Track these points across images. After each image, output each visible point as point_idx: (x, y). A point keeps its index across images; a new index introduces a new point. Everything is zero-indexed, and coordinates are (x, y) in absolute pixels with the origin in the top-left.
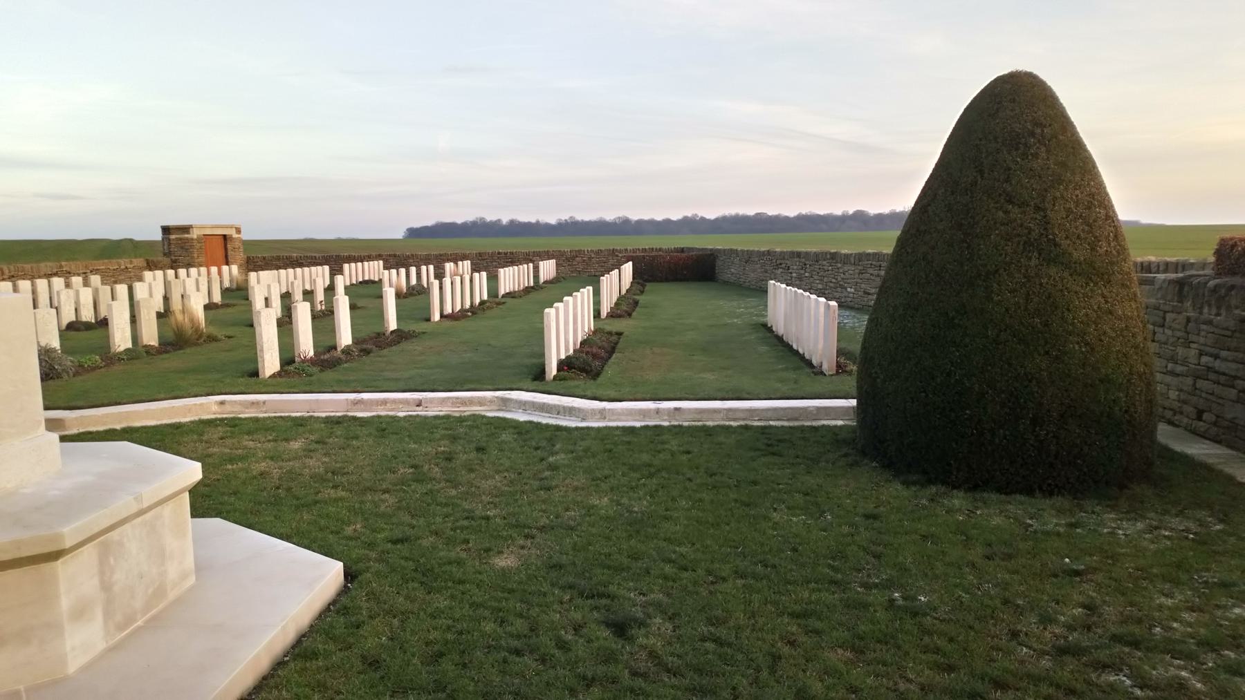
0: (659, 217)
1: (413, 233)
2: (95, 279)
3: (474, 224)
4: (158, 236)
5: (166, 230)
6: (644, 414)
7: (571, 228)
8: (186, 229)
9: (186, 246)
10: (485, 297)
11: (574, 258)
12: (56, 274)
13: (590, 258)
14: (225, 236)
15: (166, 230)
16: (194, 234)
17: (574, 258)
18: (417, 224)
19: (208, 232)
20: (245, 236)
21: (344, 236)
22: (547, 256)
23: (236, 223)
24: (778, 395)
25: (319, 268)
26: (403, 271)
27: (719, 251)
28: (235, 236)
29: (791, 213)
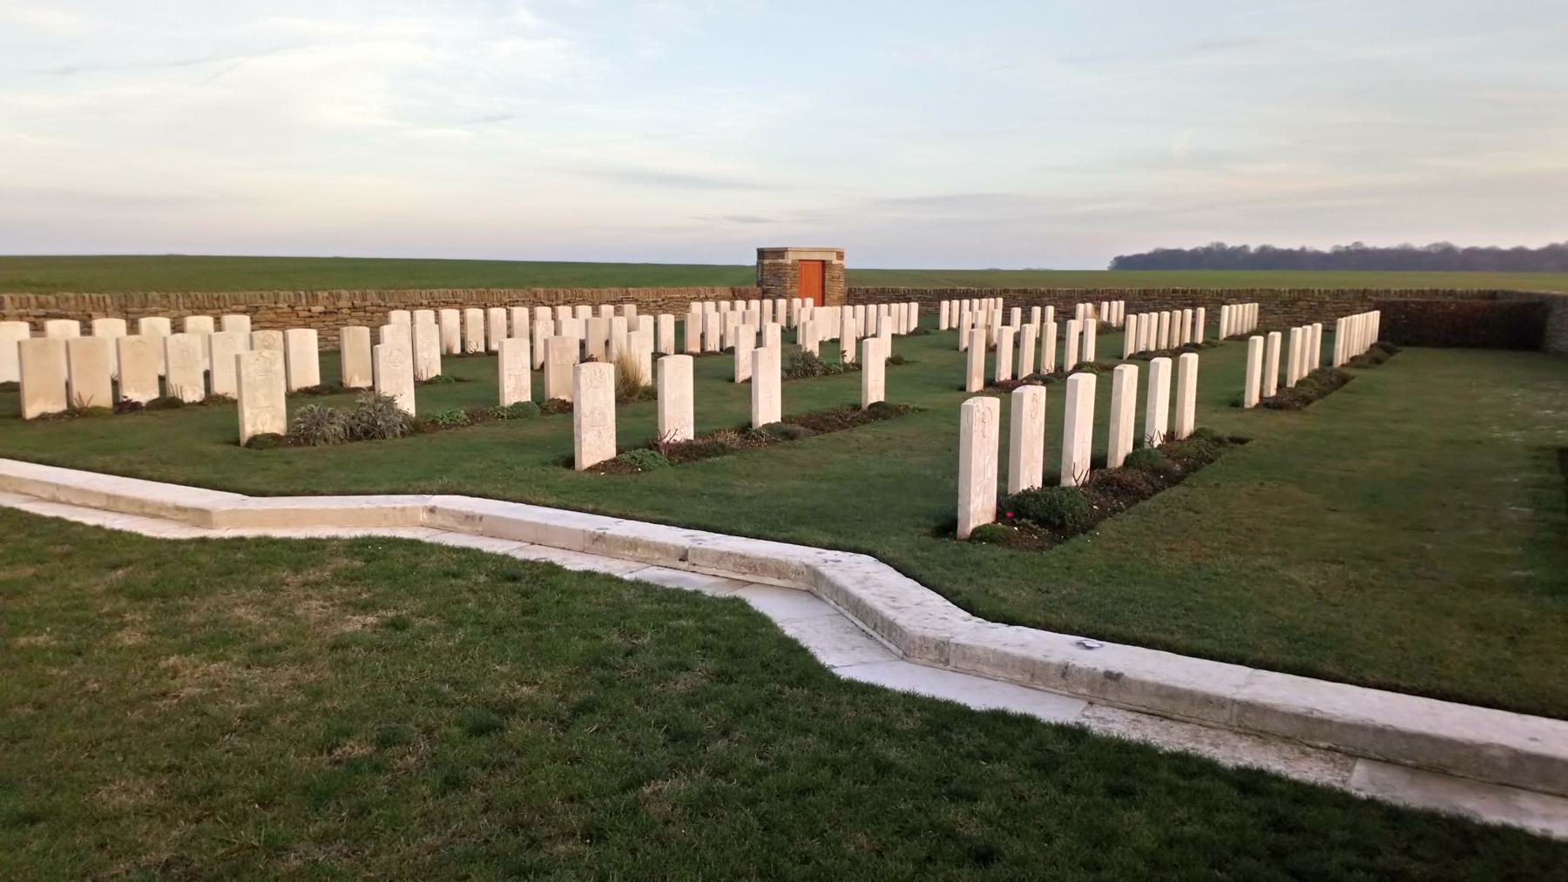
0: (1506, 244)
1: (1123, 263)
2: (630, 309)
3: (1208, 252)
4: (751, 260)
5: (762, 253)
6: (1252, 720)
7: (1269, 259)
8: (780, 253)
9: (778, 273)
10: (1316, 366)
11: (1294, 302)
12: (448, 304)
13: (1322, 304)
15: (762, 253)
16: (790, 259)
17: (1294, 302)
18: (1129, 251)
19: (805, 256)
20: (849, 263)
21: (1034, 267)
22: (1239, 297)
23: (838, 246)
24: (1421, 684)
25: (904, 306)
26: (1189, 312)
27: (1554, 298)
28: (835, 262)
29: (1324, 245)
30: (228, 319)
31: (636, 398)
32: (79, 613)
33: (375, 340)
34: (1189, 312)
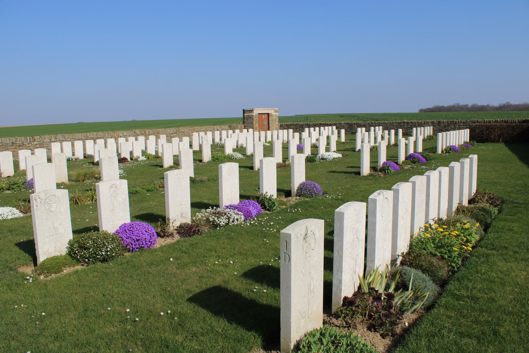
1: (421, 110)
3: (453, 107)
14: (268, 114)
18: (425, 107)
30: (208, 132)
31: (284, 168)
32: (181, 323)
33: (213, 140)
34: (393, 132)
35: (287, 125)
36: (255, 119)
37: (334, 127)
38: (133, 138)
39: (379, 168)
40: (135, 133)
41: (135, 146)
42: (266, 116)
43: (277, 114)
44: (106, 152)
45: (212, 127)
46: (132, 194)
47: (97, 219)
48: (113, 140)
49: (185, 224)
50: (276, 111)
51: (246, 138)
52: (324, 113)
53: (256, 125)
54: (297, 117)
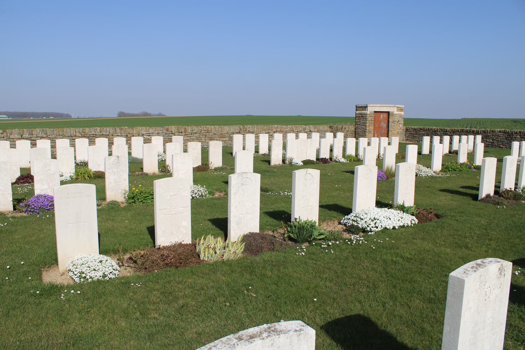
14: (388, 113)
35: (415, 129)
36: (369, 118)
37: (479, 138)
38: (86, 141)
39: (479, 198)
40: (167, 130)
41: (334, 144)
42: (385, 115)
43: (402, 113)
44: (302, 147)
45: (255, 128)
46: (263, 190)
47: (289, 200)
48: (124, 140)
49: (180, 245)
50: (401, 110)
51: (54, 157)
52: (492, 118)
53: (370, 127)
54: (464, 120)
